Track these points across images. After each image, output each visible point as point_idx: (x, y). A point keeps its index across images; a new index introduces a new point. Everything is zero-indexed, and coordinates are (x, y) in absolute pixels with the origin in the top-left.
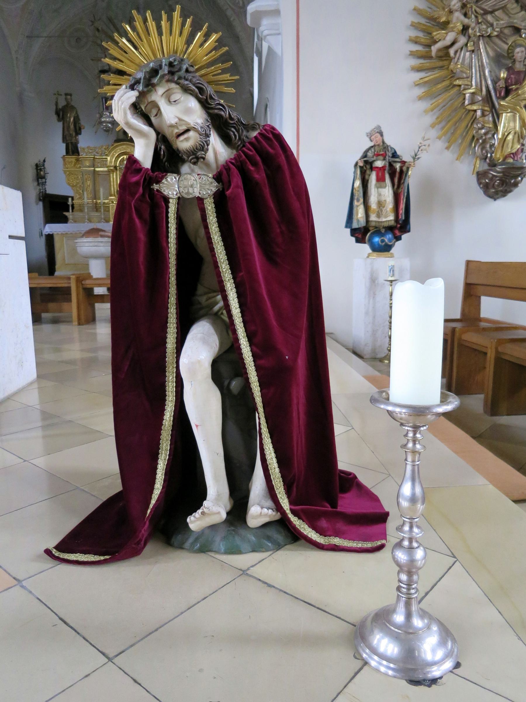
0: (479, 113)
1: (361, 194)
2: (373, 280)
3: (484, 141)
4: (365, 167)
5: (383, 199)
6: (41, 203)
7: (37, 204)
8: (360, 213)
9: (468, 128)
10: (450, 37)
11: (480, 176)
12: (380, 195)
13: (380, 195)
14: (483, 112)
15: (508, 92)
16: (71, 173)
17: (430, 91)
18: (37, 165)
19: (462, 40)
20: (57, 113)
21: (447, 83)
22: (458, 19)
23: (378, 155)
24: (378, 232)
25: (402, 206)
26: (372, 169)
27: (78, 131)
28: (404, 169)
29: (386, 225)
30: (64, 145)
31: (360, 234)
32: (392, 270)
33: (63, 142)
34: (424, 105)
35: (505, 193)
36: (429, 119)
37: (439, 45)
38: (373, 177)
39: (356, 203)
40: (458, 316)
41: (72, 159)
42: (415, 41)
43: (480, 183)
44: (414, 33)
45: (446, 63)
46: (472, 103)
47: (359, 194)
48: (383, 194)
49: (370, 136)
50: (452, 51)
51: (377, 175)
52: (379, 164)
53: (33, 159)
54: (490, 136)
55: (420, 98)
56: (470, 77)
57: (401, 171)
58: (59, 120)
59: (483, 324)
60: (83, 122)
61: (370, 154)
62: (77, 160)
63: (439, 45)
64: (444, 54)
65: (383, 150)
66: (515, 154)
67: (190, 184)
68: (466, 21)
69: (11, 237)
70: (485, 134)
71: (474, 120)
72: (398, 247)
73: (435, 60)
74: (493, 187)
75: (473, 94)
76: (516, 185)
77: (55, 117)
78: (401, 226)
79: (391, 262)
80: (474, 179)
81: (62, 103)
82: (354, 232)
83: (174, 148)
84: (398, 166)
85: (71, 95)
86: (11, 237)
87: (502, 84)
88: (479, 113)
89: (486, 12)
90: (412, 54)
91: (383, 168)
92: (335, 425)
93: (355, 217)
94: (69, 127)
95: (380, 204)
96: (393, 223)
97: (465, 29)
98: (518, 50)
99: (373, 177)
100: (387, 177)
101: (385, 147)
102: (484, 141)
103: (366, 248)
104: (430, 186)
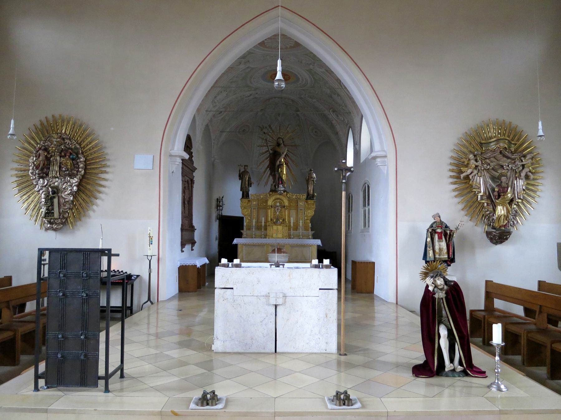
0: (485, 204)
1: (431, 245)
3: (489, 217)
4: (432, 232)
5: (442, 247)
6: (218, 221)
7: (216, 221)
8: (431, 253)
9: (480, 211)
10: (469, 171)
11: (488, 234)
12: (440, 245)
13: (440, 245)
14: (487, 204)
15: (499, 196)
16: (245, 208)
17: (460, 193)
18: (217, 199)
19: (476, 172)
20: (240, 176)
21: (469, 190)
22: (473, 163)
23: (438, 227)
25: (451, 251)
26: (436, 232)
27: (250, 184)
28: (452, 234)
29: (444, 259)
30: (241, 192)
33: (241, 190)
35: (501, 242)
36: (461, 206)
37: (464, 174)
38: (436, 236)
39: (428, 249)
40: (483, 308)
41: (246, 200)
42: (452, 171)
43: (488, 237)
44: (451, 167)
45: (468, 181)
46: (482, 199)
49: (434, 217)
50: (471, 177)
51: (438, 236)
52: (439, 230)
53: (216, 196)
54: (491, 215)
55: (456, 196)
56: (480, 188)
57: (450, 234)
58: (240, 179)
59: (497, 313)
60: (252, 180)
61: (434, 226)
62: (249, 201)
63: (464, 174)
64: (467, 177)
65: (441, 224)
66: (505, 226)
67: (440, 295)
68: (477, 164)
69: (320, 289)
70: (489, 214)
71: (483, 207)
73: (463, 181)
74: (495, 240)
75: (482, 196)
76: (507, 239)
77: (238, 177)
80: (485, 235)
81: (242, 170)
84: (448, 232)
85: (247, 166)
86: (320, 289)
87: (496, 193)
88: (485, 204)
89: (486, 159)
90: (451, 177)
91: (441, 232)
93: (428, 255)
94: (245, 183)
95: (440, 250)
96: (447, 259)
97: (477, 166)
98: (503, 178)
99: (436, 236)
100: (443, 237)
101: (442, 222)
102: (489, 217)
104: (463, 238)
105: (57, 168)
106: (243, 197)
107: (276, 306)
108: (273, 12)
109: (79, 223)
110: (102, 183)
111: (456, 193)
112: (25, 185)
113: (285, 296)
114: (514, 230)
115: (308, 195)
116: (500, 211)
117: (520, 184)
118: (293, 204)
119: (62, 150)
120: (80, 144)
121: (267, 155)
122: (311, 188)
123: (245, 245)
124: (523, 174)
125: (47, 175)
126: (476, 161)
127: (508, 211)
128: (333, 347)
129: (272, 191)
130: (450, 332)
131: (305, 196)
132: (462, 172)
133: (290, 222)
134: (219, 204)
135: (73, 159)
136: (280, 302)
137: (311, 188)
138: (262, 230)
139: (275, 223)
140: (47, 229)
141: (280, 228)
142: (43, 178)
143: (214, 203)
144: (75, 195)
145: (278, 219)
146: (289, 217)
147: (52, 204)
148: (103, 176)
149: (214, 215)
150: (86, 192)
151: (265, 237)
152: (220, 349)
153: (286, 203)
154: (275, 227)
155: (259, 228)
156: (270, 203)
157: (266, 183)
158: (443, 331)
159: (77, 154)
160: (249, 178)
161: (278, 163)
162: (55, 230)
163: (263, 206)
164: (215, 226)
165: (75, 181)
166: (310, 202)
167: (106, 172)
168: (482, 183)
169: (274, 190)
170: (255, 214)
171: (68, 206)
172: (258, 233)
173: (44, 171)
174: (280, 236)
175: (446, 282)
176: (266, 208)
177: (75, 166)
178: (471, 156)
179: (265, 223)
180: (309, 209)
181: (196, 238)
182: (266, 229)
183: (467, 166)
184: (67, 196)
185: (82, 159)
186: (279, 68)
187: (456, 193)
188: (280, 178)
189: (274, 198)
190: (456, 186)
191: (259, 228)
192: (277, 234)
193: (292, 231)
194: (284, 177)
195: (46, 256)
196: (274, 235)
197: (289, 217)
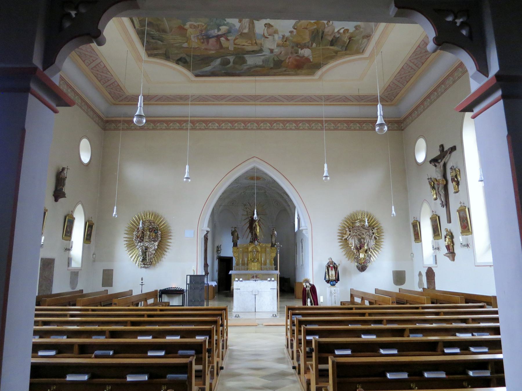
2: (331, 292)
4: (328, 267)
9: (353, 256)
10: (346, 236)
11: (357, 267)
22: (348, 232)
24: (332, 281)
27: (238, 238)
31: (328, 282)
32: (335, 290)
34: (342, 250)
35: (364, 271)
36: (344, 253)
38: (330, 269)
41: (236, 248)
47: (327, 272)
48: (332, 272)
52: (331, 266)
60: (239, 236)
64: (346, 239)
67: (308, 289)
72: (337, 285)
76: (365, 269)
78: (337, 280)
79: (335, 288)
81: (233, 230)
82: (326, 281)
83: (300, 279)
92: (385, 24)
95: (332, 275)
97: (350, 234)
99: (330, 269)
101: (332, 262)
103: (329, 285)
105: (147, 237)
106: (234, 246)
107: (255, 295)
108: (251, 160)
109: (157, 264)
110: (169, 244)
111: (341, 247)
112: (131, 246)
113: (258, 292)
114: (369, 265)
115: (272, 244)
116: (362, 256)
117: (372, 243)
118: (263, 250)
119: (150, 228)
120: (158, 225)
121: (248, 220)
122: (274, 240)
123: (236, 274)
124: (373, 237)
125: (143, 240)
126: (350, 231)
127: (365, 256)
128: (276, 309)
129: (251, 242)
130: (311, 302)
131: (270, 245)
132: (343, 237)
133: (261, 260)
134: (218, 249)
135: (156, 233)
136: (256, 293)
137: (274, 240)
138: (245, 265)
139: (253, 261)
140: (141, 267)
141: (256, 264)
142: (140, 242)
143: (215, 249)
144: (156, 250)
145: (254, 259)
146: (261, 258)
147: (146, 255)
148: (169, 241)
149: (216, 256)
150: (161, 249)
151: (247, 270)
152: (236, 311)
153: (259, 250)
154: (253, 264)
155: (243, 264)
156: (250, 249)
157: (247, 237)
158: (309, 300)
159: (157, 230)
160: (238, 235)
161: (254, 225)
162: (146, 268)
163: (246, 251)
164: (216, 262)
165: (156, 244)
166: (273, 248)
167: (171, 239)
168: (353, 242)
169: (252, 242)
170: (241, 255)
171: (152, 256)
172: (243, 267)
173: (141, 239)
174: (256, 269)
175: (310, 284)
176: (247, 252)
177: (156, 236)
178: (347, 229)
179: (247, 261)
180: (273, 252)
181: (209, 271)
182: (247, 265)
183: (345, 234)
184: (152, 250)
185: (160, 233)
186: (255, 213)
187: (341, 247)
188: (256, 234)
189: (252, 246)
190: (341, 243)
191: (243, 264)
192: (254, 267)
193: (263, 266)
194: (258, 234)
195: (189, 277)
196: (253, 269)
197: (261, 258)
